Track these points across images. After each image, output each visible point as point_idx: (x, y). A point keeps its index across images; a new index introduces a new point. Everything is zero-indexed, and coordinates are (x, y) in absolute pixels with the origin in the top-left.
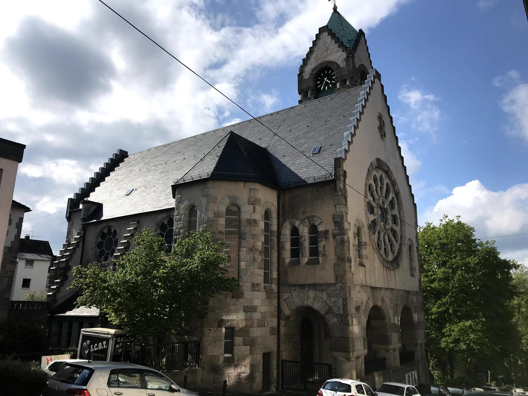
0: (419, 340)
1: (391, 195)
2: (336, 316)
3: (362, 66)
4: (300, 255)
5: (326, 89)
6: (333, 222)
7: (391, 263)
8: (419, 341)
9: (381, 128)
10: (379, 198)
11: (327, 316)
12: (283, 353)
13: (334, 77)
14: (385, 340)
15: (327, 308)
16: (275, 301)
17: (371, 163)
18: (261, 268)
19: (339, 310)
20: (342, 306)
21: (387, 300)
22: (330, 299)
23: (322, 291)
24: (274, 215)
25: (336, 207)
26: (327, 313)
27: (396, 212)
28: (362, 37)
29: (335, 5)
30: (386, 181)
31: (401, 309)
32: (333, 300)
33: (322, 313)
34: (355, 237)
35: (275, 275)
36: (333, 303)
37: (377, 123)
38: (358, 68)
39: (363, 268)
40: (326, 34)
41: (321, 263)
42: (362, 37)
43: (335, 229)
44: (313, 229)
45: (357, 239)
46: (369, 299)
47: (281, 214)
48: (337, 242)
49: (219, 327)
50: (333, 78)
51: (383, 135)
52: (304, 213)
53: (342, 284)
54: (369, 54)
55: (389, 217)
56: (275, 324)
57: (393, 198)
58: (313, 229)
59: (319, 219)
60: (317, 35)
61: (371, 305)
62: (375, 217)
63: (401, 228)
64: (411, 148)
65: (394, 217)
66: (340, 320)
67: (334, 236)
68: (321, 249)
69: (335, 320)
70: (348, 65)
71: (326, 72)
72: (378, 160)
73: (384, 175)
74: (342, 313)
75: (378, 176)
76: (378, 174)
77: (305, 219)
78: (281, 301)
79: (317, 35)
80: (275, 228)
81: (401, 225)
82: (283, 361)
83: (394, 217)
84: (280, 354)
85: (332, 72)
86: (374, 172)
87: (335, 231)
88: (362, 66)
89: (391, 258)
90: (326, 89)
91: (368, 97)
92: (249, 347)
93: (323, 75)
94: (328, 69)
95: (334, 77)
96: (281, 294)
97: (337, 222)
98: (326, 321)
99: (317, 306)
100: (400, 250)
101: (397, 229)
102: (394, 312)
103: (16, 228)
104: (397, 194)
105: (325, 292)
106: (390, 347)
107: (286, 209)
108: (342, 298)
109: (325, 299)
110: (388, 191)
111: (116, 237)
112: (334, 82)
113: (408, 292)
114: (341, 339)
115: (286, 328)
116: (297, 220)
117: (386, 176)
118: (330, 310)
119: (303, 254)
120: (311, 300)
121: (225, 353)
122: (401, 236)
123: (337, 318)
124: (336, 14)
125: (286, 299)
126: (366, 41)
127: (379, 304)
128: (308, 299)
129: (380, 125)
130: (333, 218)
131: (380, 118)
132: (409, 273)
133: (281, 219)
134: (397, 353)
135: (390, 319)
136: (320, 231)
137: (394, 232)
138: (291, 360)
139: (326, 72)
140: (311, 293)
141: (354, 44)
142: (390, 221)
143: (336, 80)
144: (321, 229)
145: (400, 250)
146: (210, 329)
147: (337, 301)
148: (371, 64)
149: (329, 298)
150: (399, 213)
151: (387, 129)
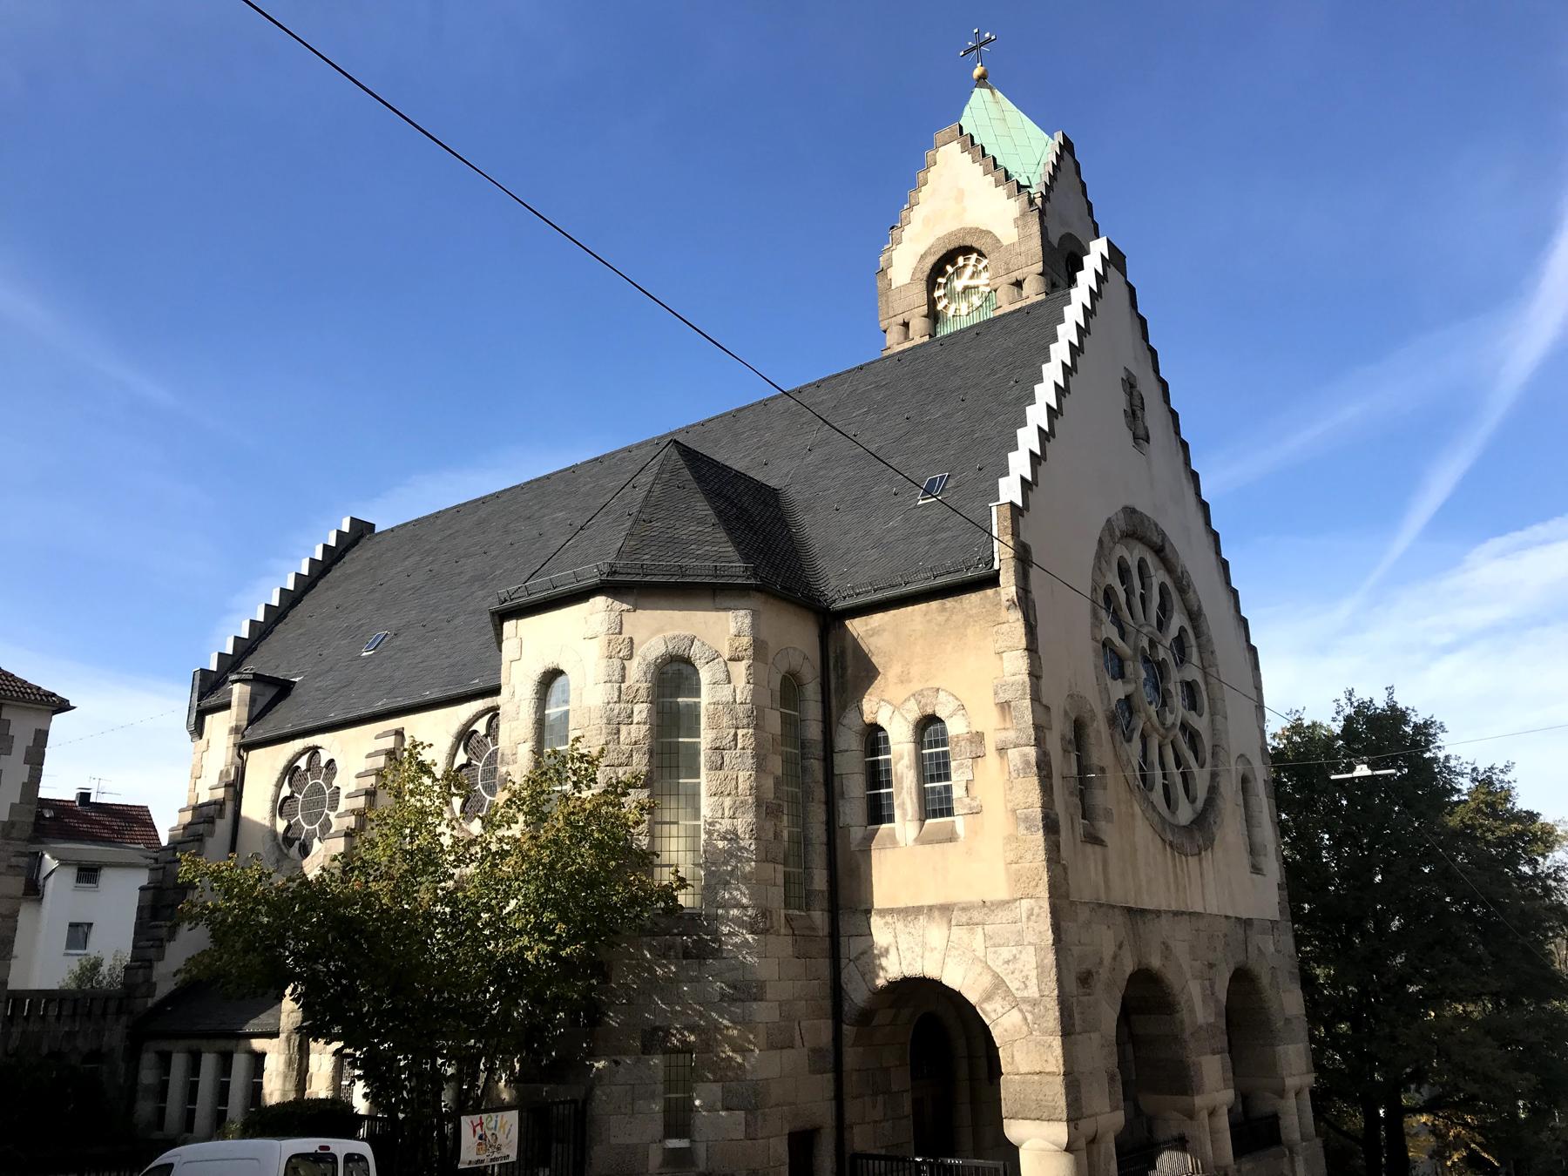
0: (1292, 1075)
1: (1177, 621)
2: (1016, 1004)
4: (897, 813)
6: (997, 704)
7: (1188, 829)
8: (1292, 1082)
9: (1134, 413)
11: (988, 1007)
12: (856, 1130)
14: (1181, 1081)
15: (987, 980)
16: (824, 966)
17: (1109, 521)
18: (774, 861)
19: (1026, 987)
20: (1034, 973)
21: (1180, 950)
22: (995, 952)
23: (971, 924)
24: (812, 690)
25: (1001, 658)
26: (988, 997)
27: (1193, 673)
30: (1158, 576)
31: (1228, 976)
32: (1006, 953)
33: (972, 998)
34: (1065, 751)
35: (820, 881)
36: (1008, 962)
37: (1122, 401)
39: (1098, 848)
41: (962, 838)
43: (1002, 726)
44: (928, 726)
45: (1073, 756)
46: (1120, 947)
47: (833, 686)
48: (1011, 769)
49: (643, 1053)
51: (1141, 437)
52: (904, 680)
53: (1032, 901)
55: (1175, 688)
56: (825, 1037)
57: (1182, 629)
58: (928, 726)
59: (951, 698)
61: (1129, 967)
62: (1130, 688)
63: (1212, 721)
65: (1190, 688)
66: (1029, 1017)
67: (1001, 750)
68: (958, 792)
69: (1015, 1016)
72: (1130, 511)
73: (1151, 559)
74: (1037, 995)
75: (1133, 564)
76: (1133, 554)
77: (908, 699)
78: (844, 962)
80: (814, 731)
81: (1213, 714)
82: (856, 1156)
83: (1190, 688)
84: (847, 1135)
86: (1121, 551)
87: (1003, 735)
89: (1185, 814)
92: (742, 1113)
94: (966, 250)
96: (843, 940)
97: (1008, 703)
98: (987, 1021)
99: (952, 980)
100: (1213, 790)
101: (1201, 724)
102: (1203, 989)
104: (1195, 616)
105: (979, 929)
106: (1199, 1101)
107: (849, 671)
108: (1032, 948)
109: (980, 953)
110: (1164, 608)
111: (335, 783)
113: (1247, 923)
114: (1036, 1077)
115: (861, 1049)
116: (882, 703)
117: (1156, 560)
118: (999, 985)
119: (906, 810)
120: (938, 956)
121: (668, 1134)
122: (1215, 746)
123: (1021, 1010)
125: (857, 958)
127: (1155, 962)
128: (927, 954)
129: (1131, 405)
130: (996, 693)
131: (1130, 384)
132: (1245, 860)
133: (834, 702)
134: (1224, 1122)
135: (1192, 1011)
136: (957, 736)
137: (1193, 738)
138: (883, 1152)
140: (935, 933)
142: (1178, 700)
144: (955, 727)
145: (1213, 790)
146: (618, 1058)
147: (1018, 956)
149: (993, 949)
150: (1204, 670)
151: (1154, 418)
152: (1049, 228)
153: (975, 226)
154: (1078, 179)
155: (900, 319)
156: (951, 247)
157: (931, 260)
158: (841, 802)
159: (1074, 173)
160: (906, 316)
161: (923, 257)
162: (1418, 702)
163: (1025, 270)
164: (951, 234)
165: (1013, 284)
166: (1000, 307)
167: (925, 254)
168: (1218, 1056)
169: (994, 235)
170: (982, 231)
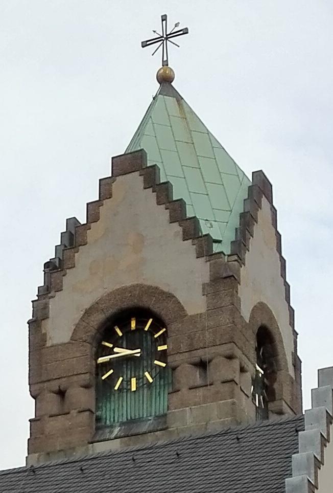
3: (261, 308)
5: (134, 389)
10: (232, 409)
13: (165, 347)
28: (264, 200)
29: (165, 63)
38: (248, 321)
40: (136, 179)
42: (264, 200)
50: (160, 348)
54: (283, 261)
60: (255, 174)
64: (332, 429)
70: (214, 309)
71: (133, 325)
79: (103, 182)
85: (155, 328)
88: (261, 308)
90: (134, 389)
91: (317, 471)
93: (121, 334)
94: (142, 314)
95: (165, 347)
103: (167, 183)
112: (164, 365)
124: (171, 100)
126: (274, 211)
139: (133, 325)
141: (236, 229)
143: (170, 359)
148: (283, 275)
152: (242, 300)
153: (154, 285)
154: (278, 255)
155: (55, 385)
156: (125, 305)
157: (98, 318)
158: (238, 226)
159: (275, 249)
160: (63, 383)
161: (88, 312)
162: (156, 204)
163: (213, 350)
164: (125, 290)
165: (195, 365)
166: (179, 391)
167: (90, 308)
168: (204, 233)
169: (177, 300)
170: (163, 293)
